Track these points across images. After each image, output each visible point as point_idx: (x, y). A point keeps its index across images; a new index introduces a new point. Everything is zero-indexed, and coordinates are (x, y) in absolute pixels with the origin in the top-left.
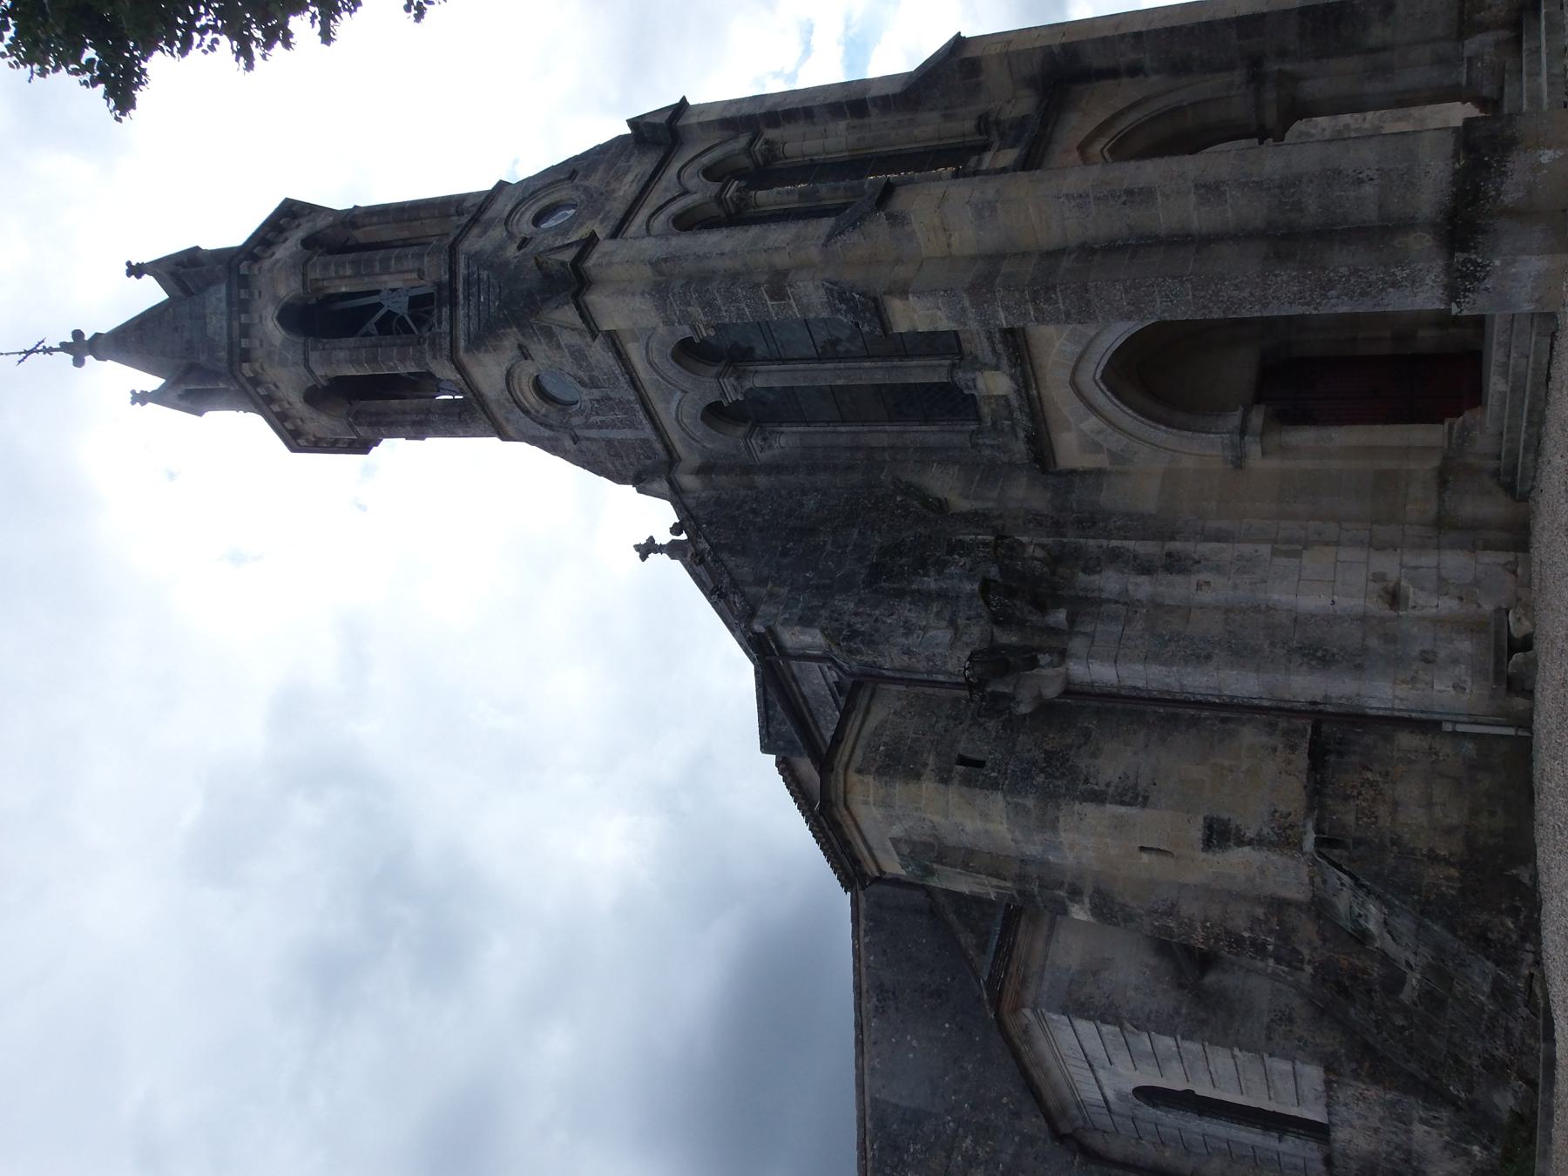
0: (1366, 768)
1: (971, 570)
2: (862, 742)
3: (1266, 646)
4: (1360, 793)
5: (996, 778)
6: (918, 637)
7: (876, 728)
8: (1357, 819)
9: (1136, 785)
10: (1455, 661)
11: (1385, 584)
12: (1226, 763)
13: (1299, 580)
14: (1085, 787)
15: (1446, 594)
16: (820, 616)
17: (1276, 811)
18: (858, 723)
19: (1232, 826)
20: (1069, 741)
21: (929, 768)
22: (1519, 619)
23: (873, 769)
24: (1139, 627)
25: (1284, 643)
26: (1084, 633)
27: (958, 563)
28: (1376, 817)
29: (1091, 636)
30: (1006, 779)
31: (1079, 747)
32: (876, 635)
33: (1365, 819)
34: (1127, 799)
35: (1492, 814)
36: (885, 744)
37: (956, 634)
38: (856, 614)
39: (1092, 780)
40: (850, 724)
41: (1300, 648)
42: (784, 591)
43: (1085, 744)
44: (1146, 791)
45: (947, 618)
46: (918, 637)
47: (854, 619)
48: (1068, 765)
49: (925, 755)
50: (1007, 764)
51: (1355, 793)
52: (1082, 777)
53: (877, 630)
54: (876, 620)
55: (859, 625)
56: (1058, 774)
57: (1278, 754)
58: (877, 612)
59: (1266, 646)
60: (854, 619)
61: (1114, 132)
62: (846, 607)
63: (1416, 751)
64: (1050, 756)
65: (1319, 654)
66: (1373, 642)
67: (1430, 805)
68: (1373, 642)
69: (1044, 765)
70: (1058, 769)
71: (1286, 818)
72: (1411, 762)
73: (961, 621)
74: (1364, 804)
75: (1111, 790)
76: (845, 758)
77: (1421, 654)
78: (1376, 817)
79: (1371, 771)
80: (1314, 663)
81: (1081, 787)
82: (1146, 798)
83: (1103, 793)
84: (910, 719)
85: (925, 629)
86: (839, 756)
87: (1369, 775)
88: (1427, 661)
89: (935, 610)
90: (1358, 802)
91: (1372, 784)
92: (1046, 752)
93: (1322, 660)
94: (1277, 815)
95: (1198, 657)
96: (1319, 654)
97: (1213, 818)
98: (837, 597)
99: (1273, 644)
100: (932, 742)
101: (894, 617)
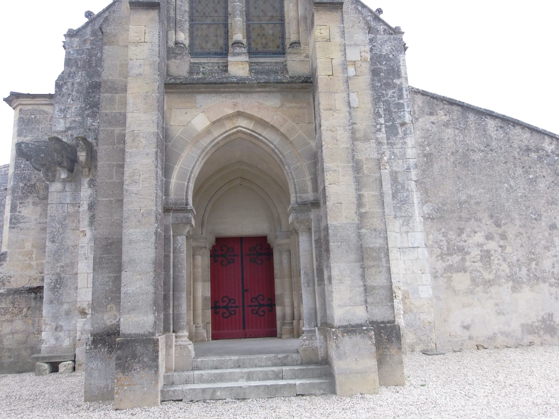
0: (29, 308)
1: (89, 129)
2: (36, 107)
3: (61, 264)
4: (16, 308)
5: (21, 167)
6: (59, 116)
7: (44, 111)
8: (3, 308)
9: (20, 223)
10: (57, 339)
11: (87, 308)
12: (34, 256)
13: (88, 273)
14: (18, 203)
15: (82, 334)
16: (72, 68)
17: (11, 277)
18: (44, 102)
19: (3, 263)
20: (41, 192)
21: (24, 139)
22: (65, 366)
23: (22, 116)
24: (70, 210)
25: (63, 271)
26: (65, 188)
27: (94, 122)
28: (4, 315)
29: (64, 190)
30: (21, 171)
31: (38, 197)
32: (60, 97)
33: (3, 311)
34: (13, 220)
35: (10, 357)
36: (35, 117)
37: (62, 132)
38: (73, 84)
39: (22, 205)
40: (42, 99)
41: (61, 278)
42: (88, 46)
43: (40, 199)
44: (17, 227)
45: (72, 126)
46: (59, 116)
47: (69, 84)
48: (28, 194)
49: (30, 135)
50: (28, 170)
51: (16, 306)
52: (23, 201)
53: (63, 96)
54: (69, 94)
55: (66, 87)
56: (24, 191)
57: (39, 274)
58: (74, 93)
59: (61, 264)
60: (69, 84)
61: (259, 130)
62: (77, 78)
63: (39, 326)
64: (34, 186)
65: (58, 286)
66: (66, 306)
67: (12, 333)
68: (66, 306)
69: (28, 185)
70: (26, 191)
71: (8, 282)
72: (33, 325)
73: (70, 132)
74: (10, 310)
75: (17, 213)
76: (24, 103)
77: (60, 326)
78: (4, 315)
79: (27, 311)
80: (53, 284)
81: (18, 202)
82: (14, 228)
83: (16, 211)
84: (447, 112)
85: (65, 117)
86: (24, 99)
87: (25, 310)
88: (56, 329)
89: (76, 119)
90: (11, 307)
91: (21, 312)
92: (35, 184)
93: (55, 287)
94: (9, 278)
95: (53, 237)
96: (58, 286)
97: (6, 255)
98: (83, 72)
99: (62, 267)
100: (38, 136)
101: (72, 101)
